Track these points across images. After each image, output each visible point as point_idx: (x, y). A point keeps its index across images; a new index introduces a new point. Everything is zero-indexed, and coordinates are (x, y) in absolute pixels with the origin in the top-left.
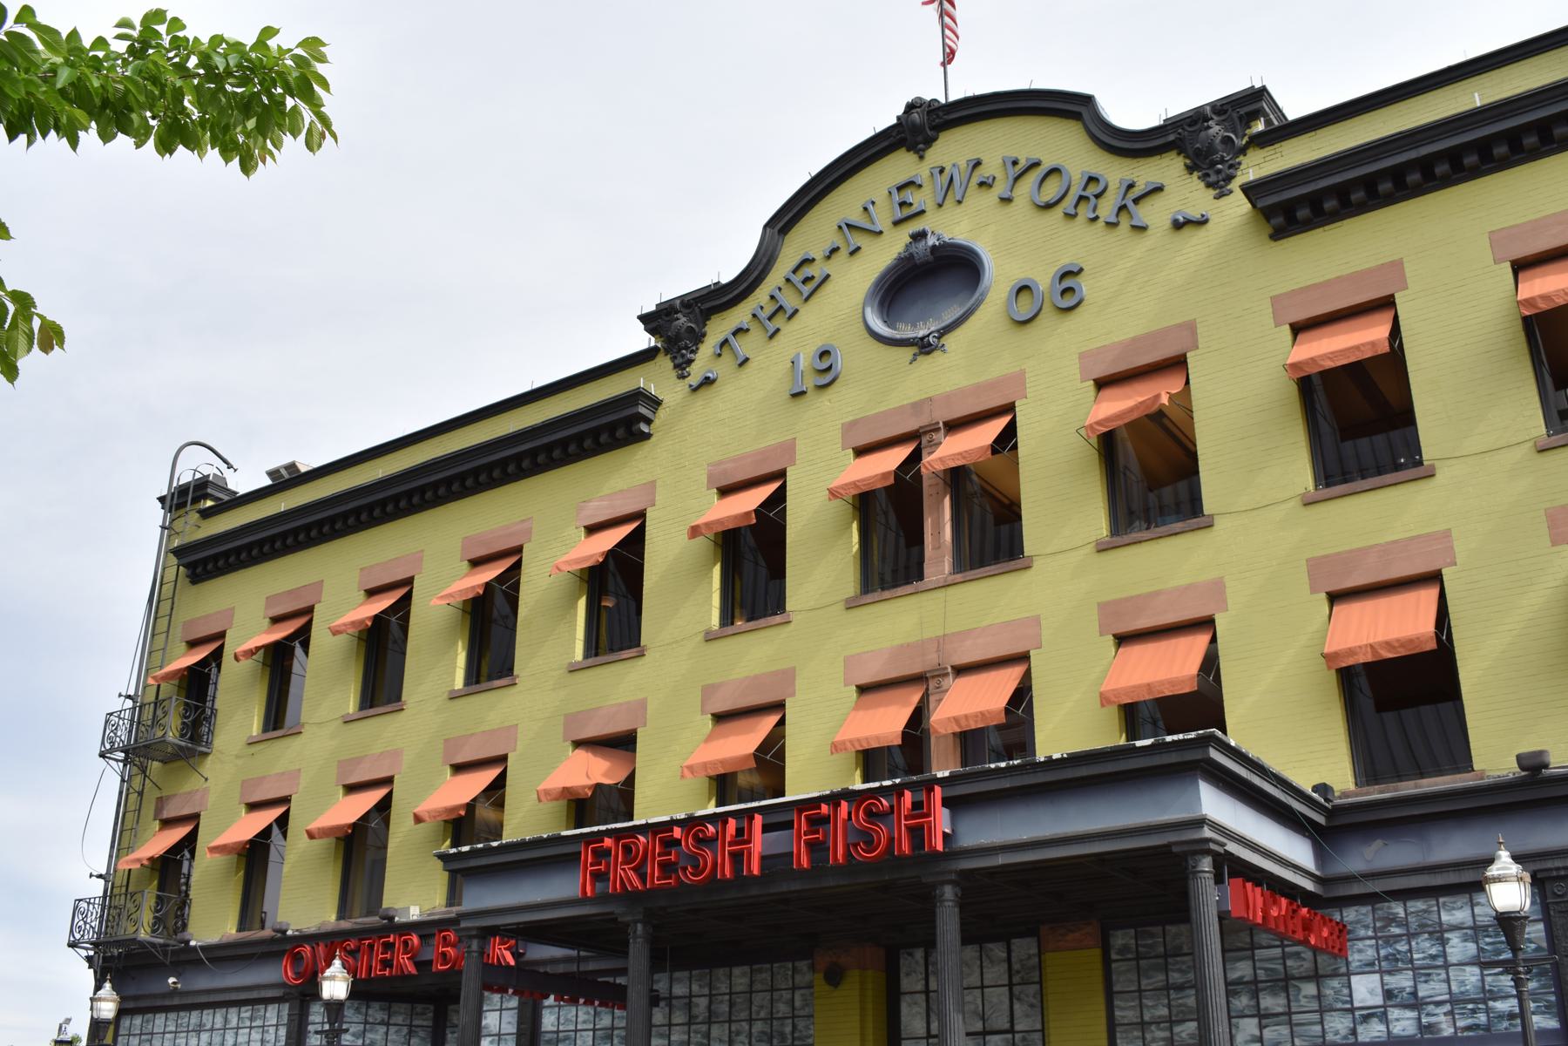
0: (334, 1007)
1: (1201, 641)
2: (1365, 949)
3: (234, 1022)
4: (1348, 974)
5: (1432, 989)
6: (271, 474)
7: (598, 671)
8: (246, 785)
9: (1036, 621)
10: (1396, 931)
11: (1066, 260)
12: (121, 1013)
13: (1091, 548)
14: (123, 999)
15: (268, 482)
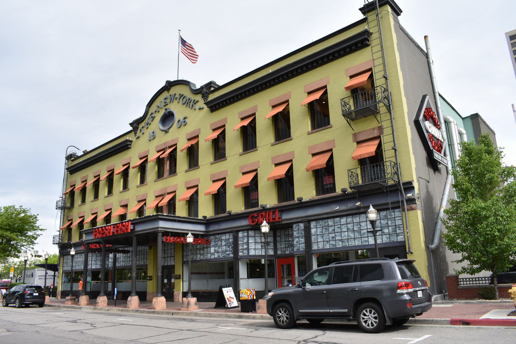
0: (73, 256)
1: (377, 142)
2: (212, 244)
3: (78, 257)
4: (211, 247)
5: (220, 250)
6: (83, 152)
7: (216, 164)
8: (92, 210)
9: (293, 152)
10: (217, 240)
11: (185, 115)
12: (76, 254)
13: (184, 172)
14: (76, 251)
15: (83, 153)
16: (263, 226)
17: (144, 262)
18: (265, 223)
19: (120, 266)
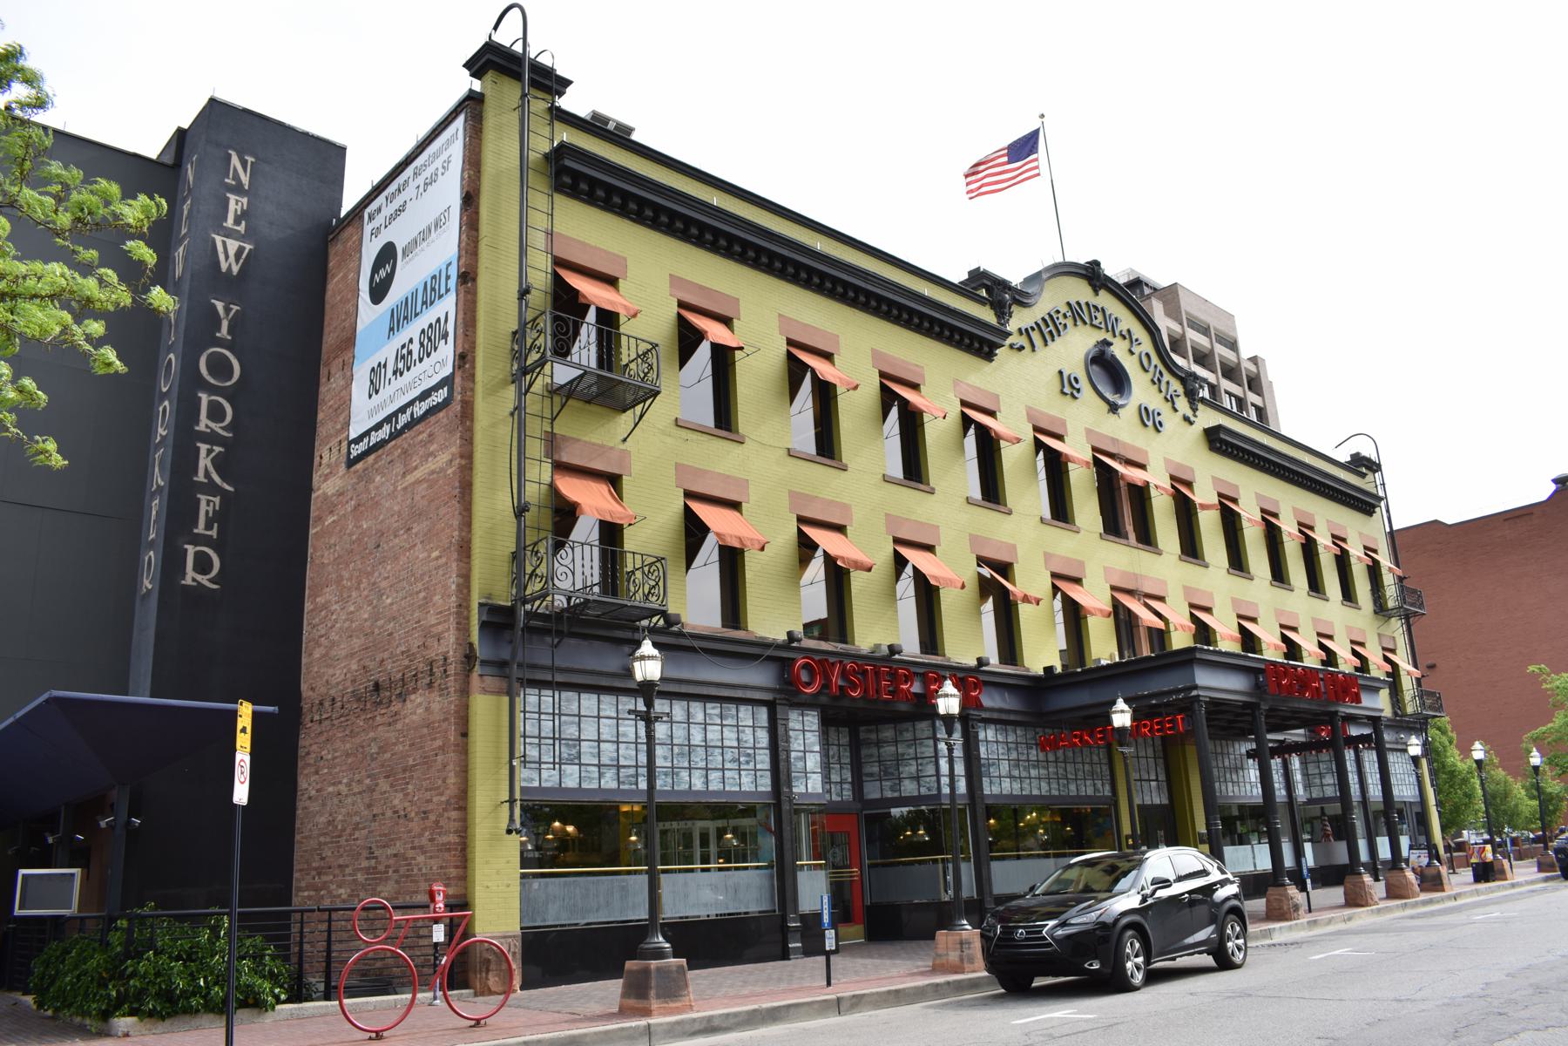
16: (1115, 712)
17: (1096, 790)
18: (1121, 704)
19: (1001, 796)
